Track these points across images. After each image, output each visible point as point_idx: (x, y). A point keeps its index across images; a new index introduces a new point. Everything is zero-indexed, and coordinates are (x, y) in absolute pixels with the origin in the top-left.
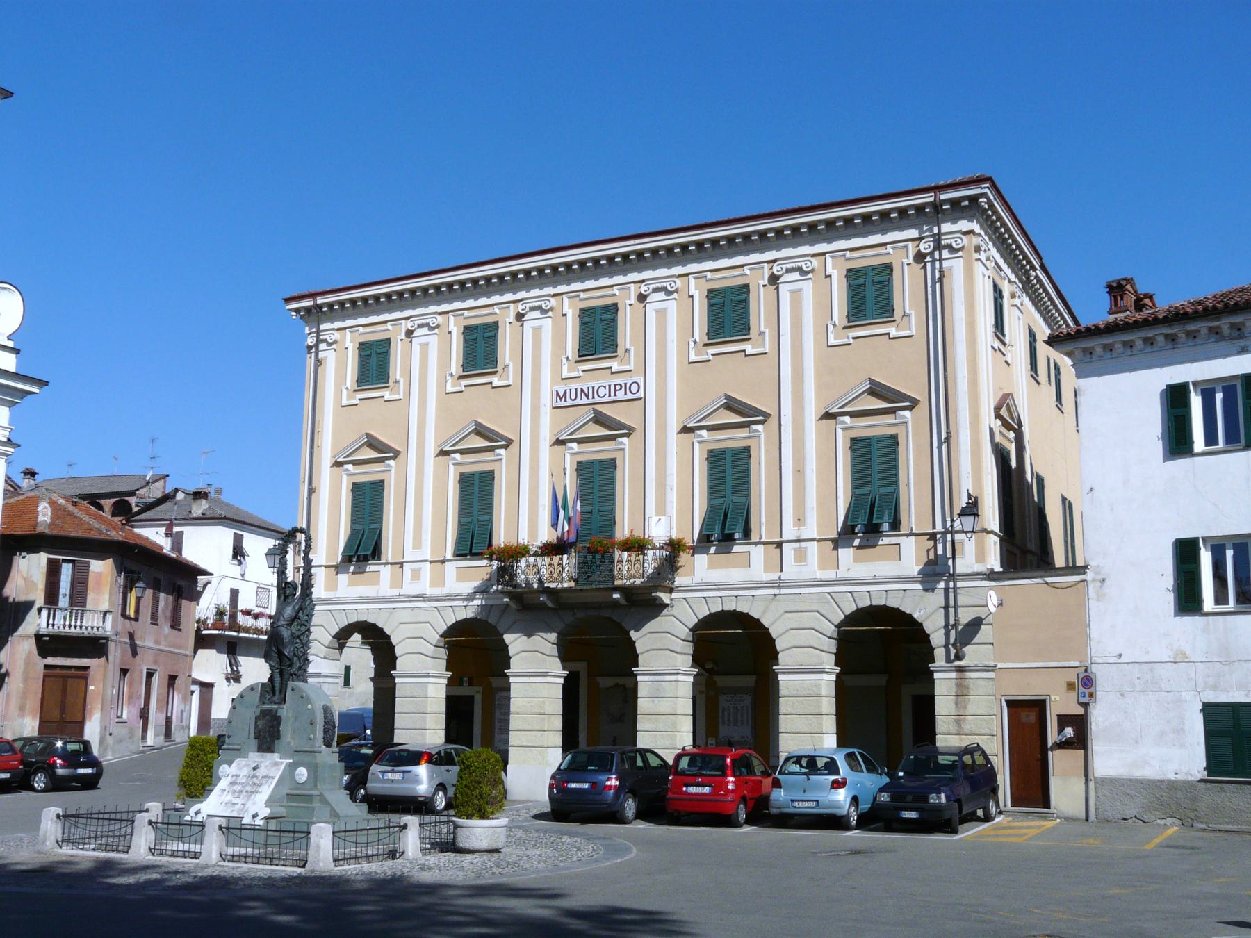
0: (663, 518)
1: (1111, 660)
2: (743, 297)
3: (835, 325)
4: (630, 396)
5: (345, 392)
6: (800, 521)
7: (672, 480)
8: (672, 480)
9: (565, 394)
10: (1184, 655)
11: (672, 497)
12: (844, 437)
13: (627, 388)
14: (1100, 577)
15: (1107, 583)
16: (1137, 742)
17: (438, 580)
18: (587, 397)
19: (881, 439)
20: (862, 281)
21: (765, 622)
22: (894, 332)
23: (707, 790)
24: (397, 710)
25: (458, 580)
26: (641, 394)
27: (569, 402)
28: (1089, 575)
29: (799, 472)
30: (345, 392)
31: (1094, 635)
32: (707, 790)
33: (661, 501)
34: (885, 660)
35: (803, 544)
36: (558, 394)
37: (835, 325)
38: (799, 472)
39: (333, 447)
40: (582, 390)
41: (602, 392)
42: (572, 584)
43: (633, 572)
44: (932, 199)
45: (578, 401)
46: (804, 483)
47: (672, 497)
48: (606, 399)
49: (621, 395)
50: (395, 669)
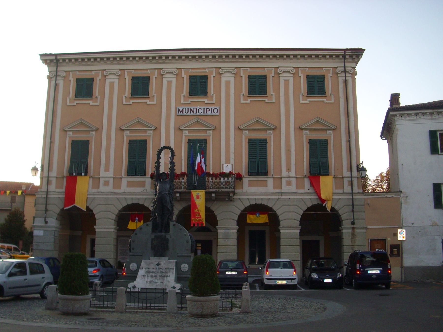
0: (229, 165)
1: (410, 225)
2: (322, 80)
3: (126, 97)
4: (213, 114)
5: (182, 98)
6: (289, 170)
7: (232, 149)
8: (232, 149)
9: (183, 109)
10: (436, 223)
11: (232, 156)
12: (306, 139)
13: (212, 111)
14: (405, 196)
15: (408, 198)
16: (419, 254)
17: (117, 185)
18: (193, 112)
19: (321, 140)
20: (313, 80)
21: (275, 209)
22: (267, 101)
23: (235, 273)
24: (96, 243)
25: (127, 186)
26: (218, 114)
27: (184, 114)
28: (402, 195)
29: (288, 150)
30: (182, 98)
31: (404, 216)
32: (235, 273)
33: (227, 156)
34: (321, 222)
35: (290, 179)
36: (179, 110)
37: (126, 97)
38: (288, 150)
39: (117, 124)
40: (191, 109)
41: (200, 111)
42: (185, 190)
43: (214, 186)
44: (343, 53)
45: (189, 114)
46: (288, 155)
47: (232, 156)
48: (202, 114)
49: (209, 113)
50: (95, 225)
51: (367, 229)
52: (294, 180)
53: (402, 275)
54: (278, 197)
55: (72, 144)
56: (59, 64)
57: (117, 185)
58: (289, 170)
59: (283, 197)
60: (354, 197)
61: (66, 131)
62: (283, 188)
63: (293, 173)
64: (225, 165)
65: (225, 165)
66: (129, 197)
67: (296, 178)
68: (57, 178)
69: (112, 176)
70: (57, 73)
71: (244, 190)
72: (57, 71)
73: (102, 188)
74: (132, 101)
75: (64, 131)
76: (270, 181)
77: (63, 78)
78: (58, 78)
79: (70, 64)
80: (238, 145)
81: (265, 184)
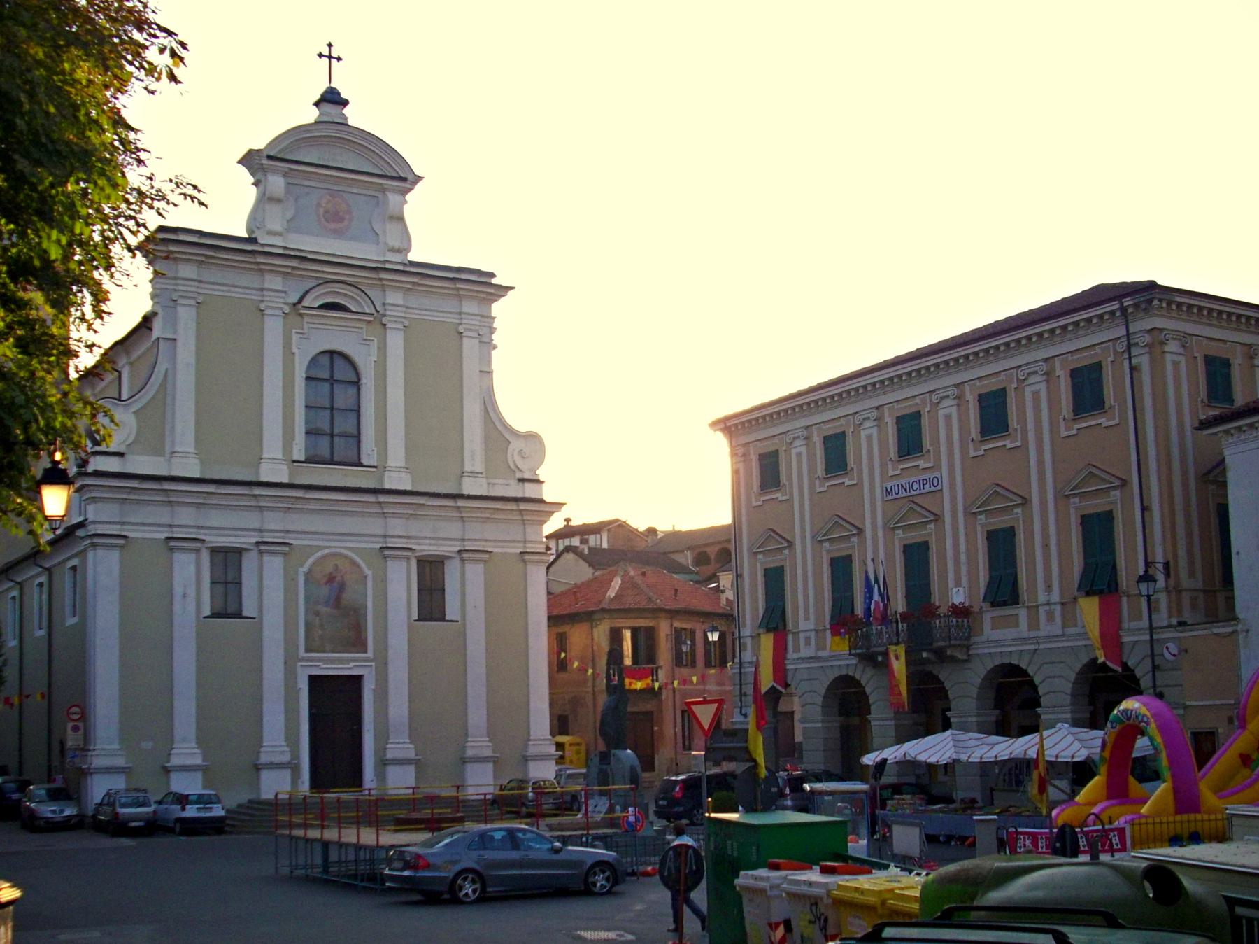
4: (933, 488)
5: (1062, 424)
6: (1049, 588)
26: (939, 488)
35: (1053, 607)
38: (1046, 546)
51: (1185, 707)
52: (1058, 608)
53: (49, 754)
54: (1033, 647)
55: (904, 552)
56: (1130, 318)
57: (1070, 617)
58: (1049, 588)
59: (1042, 646)
60: (1155, 637)
61: (1068, 496)
62: (1042, 626)
63: (1055, 596)
64: (955, 590)
65: (955, 590)
66: (1080, 643)
67: (1063, 604)
68: (1205, 591)
69: (812, 627)
70: (1128, 340)
71: (984, 638)
72: (1128, 335)
73: (1045, 629)
74: (984, 448)
75: (971, 515)
76: (1022, 613)
77: (1147, 349)
78: (1134, 351)
79: (1080, 333)
80: (1062, 531)
81: (1014, 622)
